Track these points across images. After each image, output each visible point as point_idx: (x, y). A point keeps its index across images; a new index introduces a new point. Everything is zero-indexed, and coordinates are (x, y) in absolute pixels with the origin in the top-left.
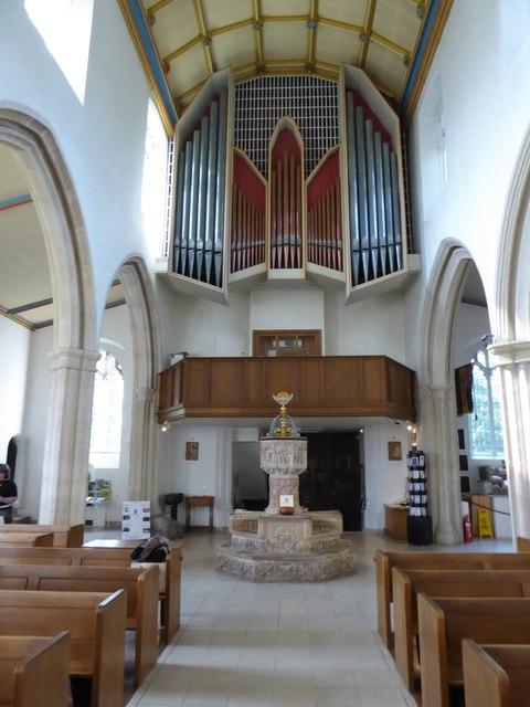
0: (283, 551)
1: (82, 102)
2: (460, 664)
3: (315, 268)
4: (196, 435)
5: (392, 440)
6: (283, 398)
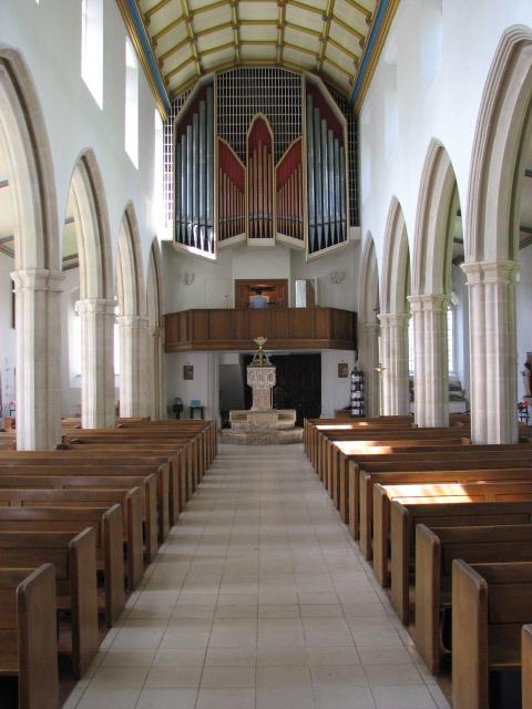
1: (101, 108)
2: (450, 589)
3: (282, 237)
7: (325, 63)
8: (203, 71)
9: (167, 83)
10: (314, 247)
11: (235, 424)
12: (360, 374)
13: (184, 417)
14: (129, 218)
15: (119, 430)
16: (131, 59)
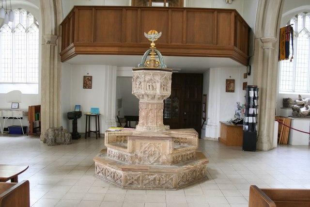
0: (147, 163)
5: (229, 78)
6: (153, 36)
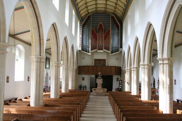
1: (58, 11)
3: (105, 50)
4: (84, 76)
7: (115, 12)
8: (89, 13)
9: (81, 16)
10: (112, 53)
11: (93, 91)
12: (121, 81)
13: (82, 88)
14: (72, 47)
15: (70, 93)
16: (74, 13)
